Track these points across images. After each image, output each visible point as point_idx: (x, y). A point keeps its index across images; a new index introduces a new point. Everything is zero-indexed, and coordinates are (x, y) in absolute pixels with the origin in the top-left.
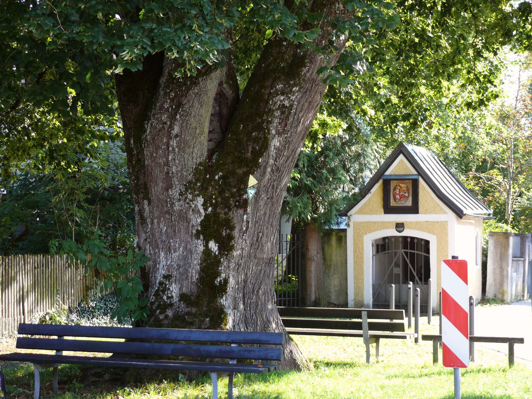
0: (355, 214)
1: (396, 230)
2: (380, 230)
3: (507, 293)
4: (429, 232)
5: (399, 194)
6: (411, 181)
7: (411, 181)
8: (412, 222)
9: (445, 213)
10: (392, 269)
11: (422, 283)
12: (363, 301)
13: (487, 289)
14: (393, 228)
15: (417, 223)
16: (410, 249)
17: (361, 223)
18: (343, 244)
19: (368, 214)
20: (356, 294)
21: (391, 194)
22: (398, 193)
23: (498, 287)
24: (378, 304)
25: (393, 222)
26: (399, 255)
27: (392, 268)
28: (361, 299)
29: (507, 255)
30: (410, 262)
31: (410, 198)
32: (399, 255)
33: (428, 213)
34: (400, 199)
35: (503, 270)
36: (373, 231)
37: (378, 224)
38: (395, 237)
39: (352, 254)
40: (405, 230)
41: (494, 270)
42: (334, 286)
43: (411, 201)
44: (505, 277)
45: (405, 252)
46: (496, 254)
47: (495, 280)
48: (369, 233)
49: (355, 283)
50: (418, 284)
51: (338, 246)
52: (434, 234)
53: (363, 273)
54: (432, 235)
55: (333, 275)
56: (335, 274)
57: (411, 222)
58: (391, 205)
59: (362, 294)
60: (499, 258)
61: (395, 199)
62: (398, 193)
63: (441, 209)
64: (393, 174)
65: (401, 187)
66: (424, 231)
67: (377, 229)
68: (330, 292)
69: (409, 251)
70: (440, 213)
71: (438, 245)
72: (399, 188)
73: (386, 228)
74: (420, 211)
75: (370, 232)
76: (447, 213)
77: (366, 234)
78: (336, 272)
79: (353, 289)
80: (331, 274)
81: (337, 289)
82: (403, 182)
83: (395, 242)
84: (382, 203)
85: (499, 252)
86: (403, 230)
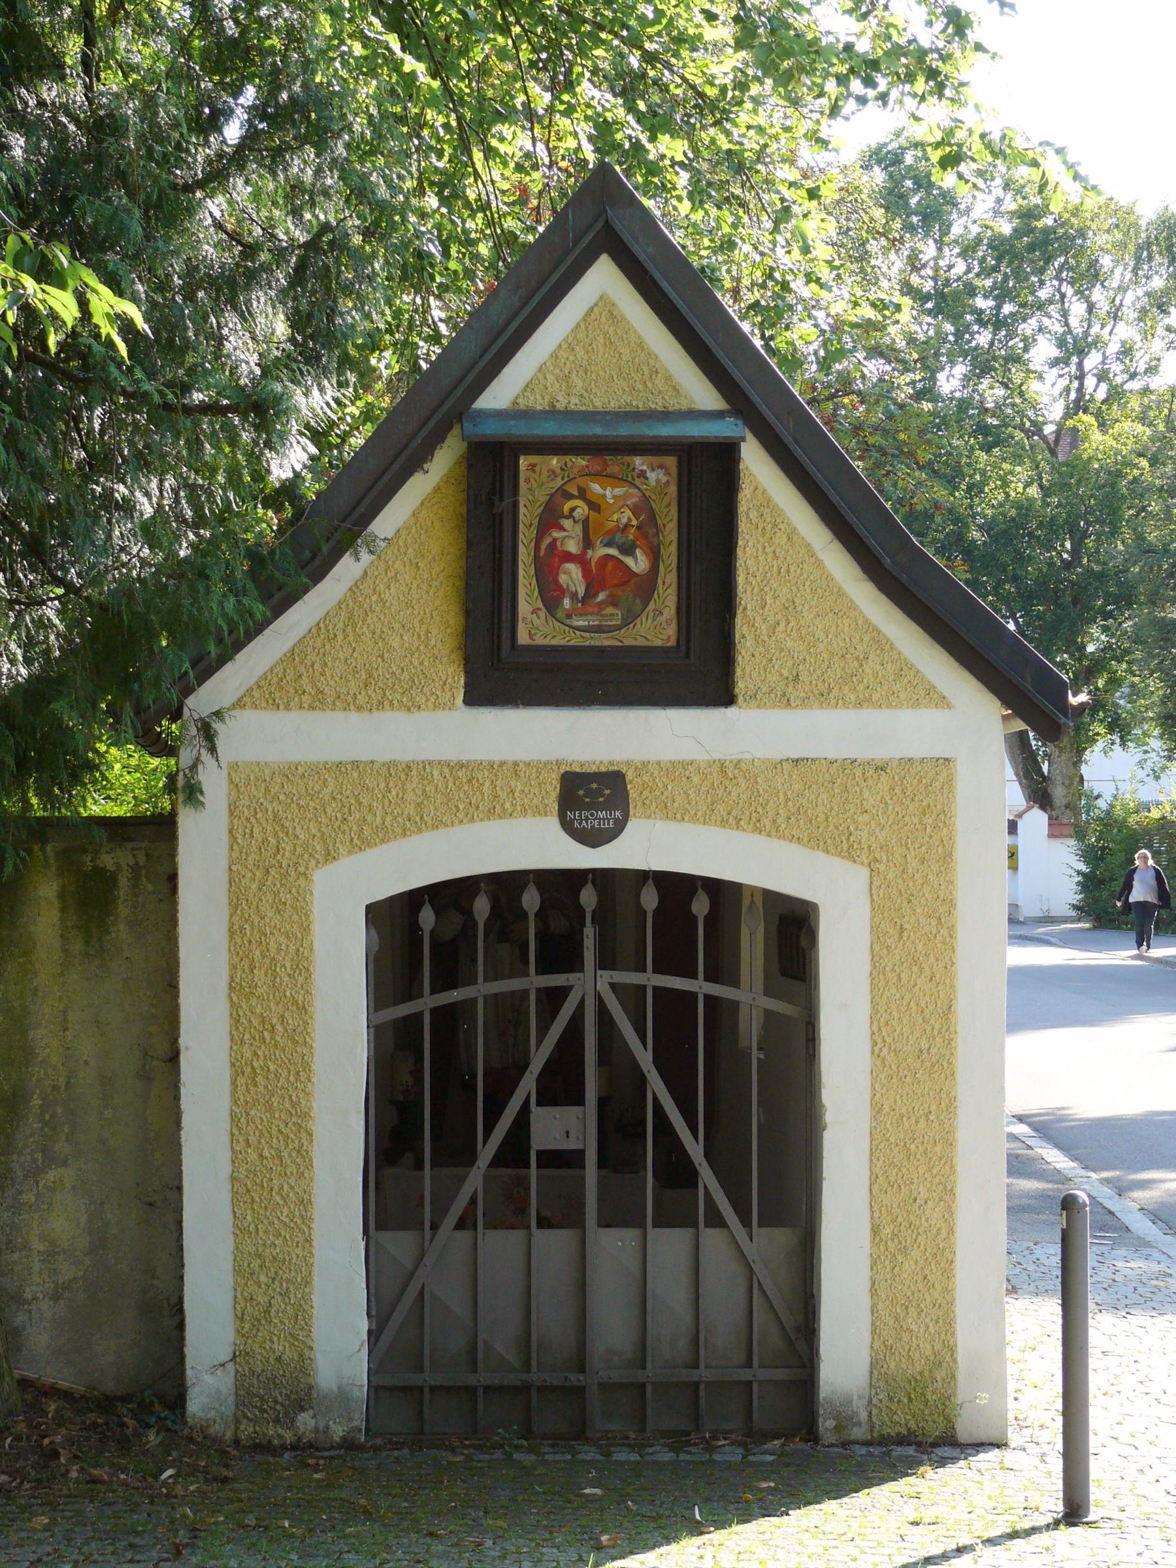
0: (239, 704)
1: (567, 826)
2: (438, 824)
4: (817, 842)
5: (580, 560)
6: (671, 462)
7: (671, 462)
8: (686, 764)
9: (935, 699)
10: (522, 1120)
11: (746, 1222)
12: (304, 1364)
14: (540, 811)
17: (289, 772)
19: (345, 702)
21: (525, 555)
24: (415, 1379)
26: (581, 1005)
27: (525, 1107)
28: (289, 1355)
30: (656, 1062)
31: (667, 596)
32: (581, 1005)
33: (804, 703)
34: (590, 594)
36: (384, 835)
37: (426, 779)
38: (573, 879)
39: (222, 1007)
42: (51, 1255)
43: (670, 611)
49: (240, 1230)
50: (716, 1220)
51: (77, 946)
52: (850, 855)
53: (303, 1155)
55: (34, 1173)
57: (679, 770)
58: (523, 638)
59: (302, 1315)
61: (551, 595)
62: (573, 547)
63: (904, 668)
64: (538, 402)
65: (594, 506)
66: (775, 831)
67: (471, 813)
68: (17, 1299)
69: (700, 986)
70: (890, 701)
71: (875, 930)
72: (582, 509)
73: (491, 813)
75: (361, 844)
76: (944, 702)
77: (330, 856)
81: (67, 1271)
82: (614, 464)
83: (712, 920)
84: (455, 620)
86: (619, 828)
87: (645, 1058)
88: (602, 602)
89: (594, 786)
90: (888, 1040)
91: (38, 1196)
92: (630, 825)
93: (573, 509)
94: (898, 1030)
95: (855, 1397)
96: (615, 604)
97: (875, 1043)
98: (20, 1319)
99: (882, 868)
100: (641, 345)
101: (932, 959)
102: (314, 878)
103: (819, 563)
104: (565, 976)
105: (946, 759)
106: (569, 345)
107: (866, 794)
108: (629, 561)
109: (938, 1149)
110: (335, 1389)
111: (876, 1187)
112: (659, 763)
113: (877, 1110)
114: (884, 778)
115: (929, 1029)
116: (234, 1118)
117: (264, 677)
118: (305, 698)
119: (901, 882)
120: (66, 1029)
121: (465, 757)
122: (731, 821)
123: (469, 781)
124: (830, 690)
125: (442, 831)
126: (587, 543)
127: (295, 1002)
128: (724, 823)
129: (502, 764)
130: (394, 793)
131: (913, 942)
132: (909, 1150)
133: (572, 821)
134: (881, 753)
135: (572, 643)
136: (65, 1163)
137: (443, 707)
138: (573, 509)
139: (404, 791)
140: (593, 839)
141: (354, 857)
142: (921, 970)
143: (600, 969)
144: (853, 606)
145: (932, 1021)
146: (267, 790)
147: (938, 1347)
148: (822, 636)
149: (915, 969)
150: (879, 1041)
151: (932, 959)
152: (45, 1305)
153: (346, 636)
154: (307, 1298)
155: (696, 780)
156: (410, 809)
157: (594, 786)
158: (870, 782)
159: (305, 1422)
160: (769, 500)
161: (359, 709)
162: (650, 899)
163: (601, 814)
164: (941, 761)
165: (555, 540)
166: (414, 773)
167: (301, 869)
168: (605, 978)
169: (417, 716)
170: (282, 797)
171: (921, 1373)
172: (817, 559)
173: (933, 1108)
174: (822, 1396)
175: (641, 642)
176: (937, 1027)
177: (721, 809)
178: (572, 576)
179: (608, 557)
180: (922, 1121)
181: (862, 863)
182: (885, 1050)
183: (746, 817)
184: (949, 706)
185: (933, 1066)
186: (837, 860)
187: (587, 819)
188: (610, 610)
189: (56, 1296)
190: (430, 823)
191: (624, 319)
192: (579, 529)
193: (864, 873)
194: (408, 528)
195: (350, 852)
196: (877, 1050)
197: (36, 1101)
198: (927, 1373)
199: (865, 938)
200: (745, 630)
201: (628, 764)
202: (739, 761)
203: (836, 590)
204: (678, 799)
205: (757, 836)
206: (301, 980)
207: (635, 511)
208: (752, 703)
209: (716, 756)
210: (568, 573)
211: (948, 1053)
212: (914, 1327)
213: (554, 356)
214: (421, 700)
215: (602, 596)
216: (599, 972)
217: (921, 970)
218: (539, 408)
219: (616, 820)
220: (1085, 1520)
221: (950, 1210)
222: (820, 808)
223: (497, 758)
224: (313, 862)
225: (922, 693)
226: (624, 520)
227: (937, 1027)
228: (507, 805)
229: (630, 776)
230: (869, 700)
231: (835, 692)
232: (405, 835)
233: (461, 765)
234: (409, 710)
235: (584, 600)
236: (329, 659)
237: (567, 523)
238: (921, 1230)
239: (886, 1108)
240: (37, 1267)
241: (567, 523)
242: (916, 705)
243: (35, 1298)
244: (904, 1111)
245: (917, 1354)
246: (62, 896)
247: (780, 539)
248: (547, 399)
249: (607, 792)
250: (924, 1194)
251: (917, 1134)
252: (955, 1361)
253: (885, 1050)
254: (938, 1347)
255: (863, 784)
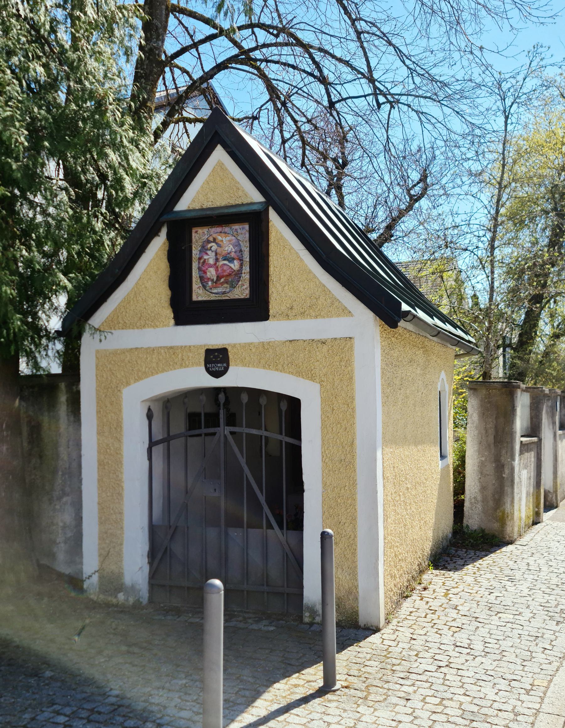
1: (207, 370)
2: (163, 371)
3: (513, 519)
4: (299, 374)
11: (281, 527)
12: (120, 575)
13: (465, 509)
14: (198, 364)
15: (265, 346)
16: (248, 426)
18: (63, 409)
19: (133, 326)
20: (104, 556)
21: (195, 265)
22: (211, 261)
23: (491, 503)
25: (198, 347)
29: (511, 434)
35: (503, 466)
36: (146, 375)
37: (159, 353)
40: (231, 369)
41: (482, 465)
42: (64, 528)
43: (247, 285)
44: (507, 483)
45: (232, 433)
46: (486, 432)
47: (483, 488)
48: (136, 380)
50: (270, 526)
51: (72, 419)
52: (312, 378)
53: (120, 495)
54: (308, 383)
55: (60, 498)
56: (64, 494)
58: (195, 298)
60: (491, 439)
63: (335, 300)
64: (197, 206)
66: (283, 370)
70: (329, 315)
71: (323, 411)
73: (181, 366)
74: (271, 312)
77: (128, 384)
78: (67, 489)
79: (96, 540)
80: (56, 494)
85: (491, 425)
87: (243, 461)
88: (223, 282)
89: (216, 354)
90: (328, 456)
91: (61, 506)
92: (231, 368)
93: (211, 247)
94: (332, 452)
95: (317, 604)
96: (227, 283)
97: (323, 457)
98: (55, 550)
99: (324, 384)
100: (233, 179)
101: (345, 421)
102: (123, 392)
103: (302, 260)
104: (213, 429)
105: (350, 338)
106: (207, 182)
107: (318, 353)
108: (232, 265)
109: (349, 502)
110: (131, 585)
111: (324, 516)
112: (240, 344)
113: (325, 485)
114: (325, 347)
115: (345, 451)
116: (99, 481)
117: (107, 318)
118: (120, 325)
119: (332, 389)
120: (69, 448)
121: (173, 345)
122: (267, 366)
123: (174, 354)
124: (305, 311)
125: (165, 373)
126: (217, 260)
127: (117, 437)
128: (264, 367)
129: (185, 347)
130: (149, 359)
131: (338, 415)
132: (337, 501)
133: (209, 368)
134: (323, 337)
135: (212, 299)
136: (68, 495)
137: (166, 326)
138: (211, 247)
139: (152, 358)
140: (217, 374)
141: (136, 384)
142: (341, 426)
143: (227, 426)
144: (315, 276)
145: (346, 448)
146: (108, 360)
147: (351, 586)
148: (302, 290)
149: (339, 426)
150: (325, 456)
151: (345, 421)
152: (62, 545)
153: (134, 301)
154: (121, 550)
155: (254, 350)
156: (154, 365)
157: (216, 354)
158: (319, 349)
159: (121, 596)
160: (282, 236)
161: (138, 328)
162: (245, 398)
163: (219, 365)
164: (348, 339)
165: (205, 260)
166: (155, 351)
167: (119, 389)
168: (228, 429)
169: (157, 329)
170: (112, 362)
171: (343, 596)
172: (301, 259)
173: (347, 484)
174: (304, 602)
175: (237, 297)
176: (348, 450)
177: (263, 361)
178: (212, 273)
179: (225, 264)
180: (342, 490)
181: (317, 382)
182: (327, 460)
183: (272, 365)
184: (352, 316)
185: (346, 466)
186: (307, 381)
187: (214, 367)
188: (225, 285)
189: (65, 543)
190: (160, 370)
191: (227, 169)
192: (214, 254)
193: (318, 386)
194: (154, 259)
195: (135, 382)
196: (324, 459)
197: (60, 473)
198: (346, 596)
199: (319, 413)
200: (273, 290)
201: (229, 345)
202: (270, 342)
203: (308, 271)
204: (247, 358)
205: (276, 372)
206: (119, 430)
207: (234, 246)
208: (274, 319)
209: (261, 341)
210: (210, 272)
211: (353, 461)
212: (340, 576)
213: (202, 187)
214: (158, 324)
215: (222, 280)
216: (226, 427)
217: (341, 426)
218: (197, 208)
219: (224, 367)
220: (333, 689)
221: (355, 528)
222: (300, 360)
223: (184, 345)
224: (122, 386)
225: (341, 311)
226: (230, 250)
227: (348, 450)
228: (187, 363)
229: (229, 349)
230: (320, 315)
231: (307, 313)
232: (152, 375)
233: (171, 348)
234: (154, 327)
235: (216, 283)
236: (128, 310)
237: (209, 252)
238: (343, 536)
239: (328, 483)
240: (60, 531)
241: (209, 252)
242: (339, 316)
243: (60, 543)
244: (335, 485)
245: (342, 588)
246: (67, 401)
247: (287, 252)
248: (200, 204)
249: (221, 356)
250: (344, 521)
251: (341, 495)
252: (358, 592)
253: (327, 460)
254: (351, 586)
255: (317, 350)
